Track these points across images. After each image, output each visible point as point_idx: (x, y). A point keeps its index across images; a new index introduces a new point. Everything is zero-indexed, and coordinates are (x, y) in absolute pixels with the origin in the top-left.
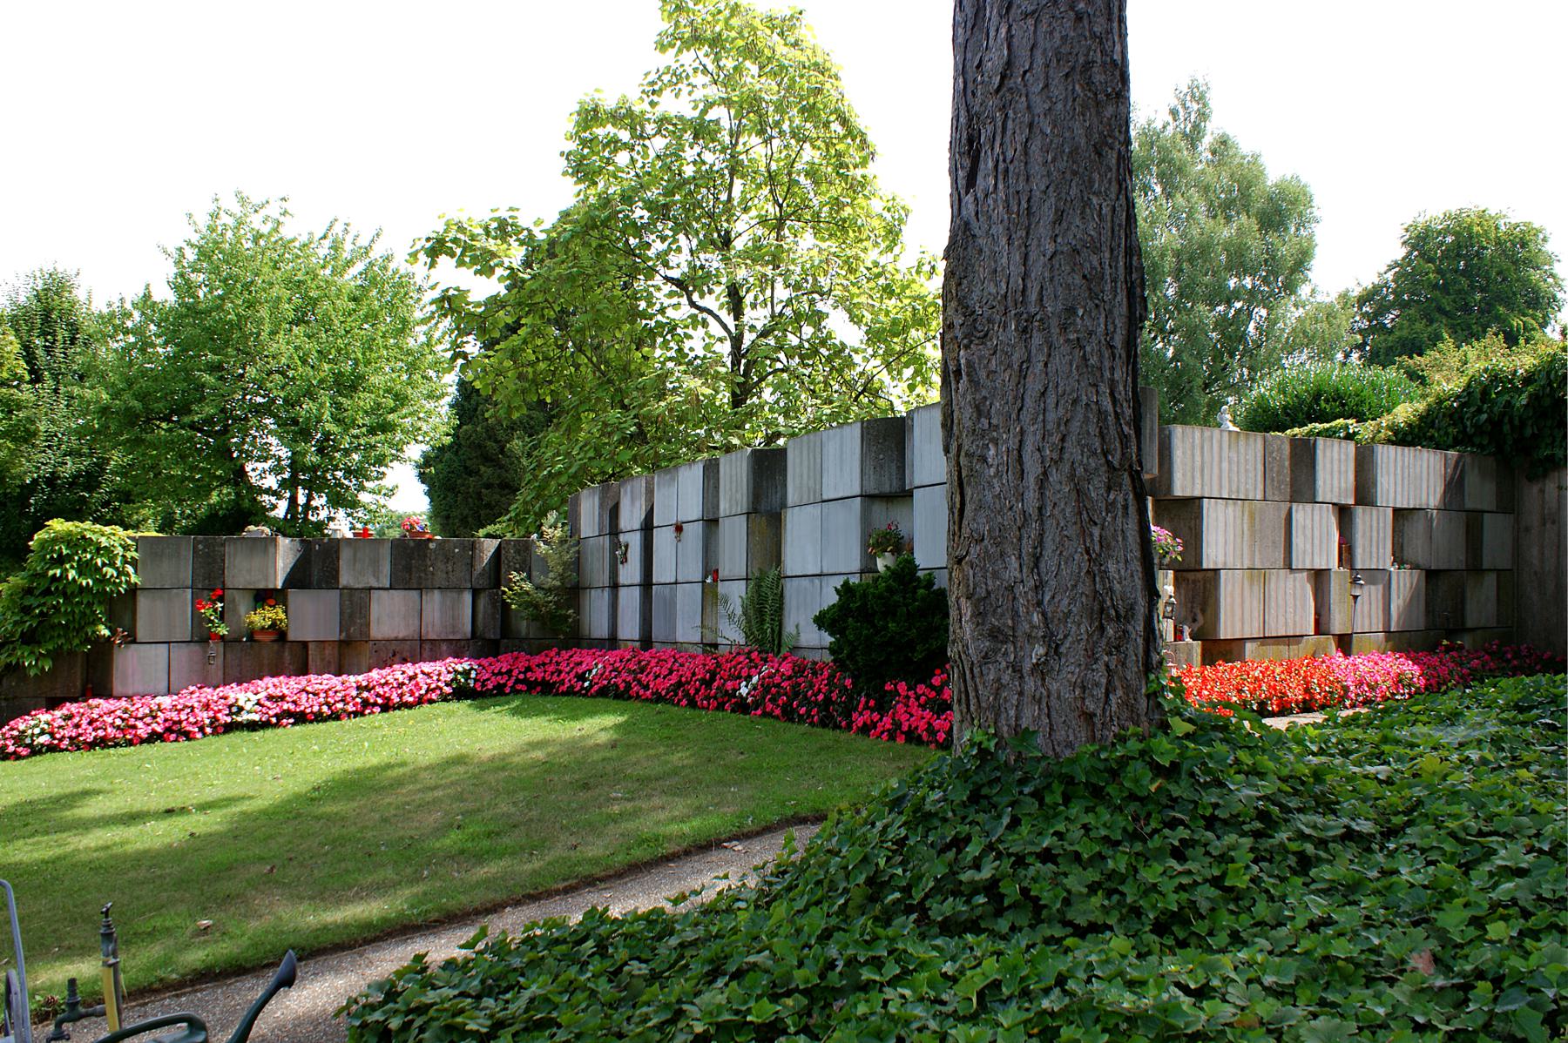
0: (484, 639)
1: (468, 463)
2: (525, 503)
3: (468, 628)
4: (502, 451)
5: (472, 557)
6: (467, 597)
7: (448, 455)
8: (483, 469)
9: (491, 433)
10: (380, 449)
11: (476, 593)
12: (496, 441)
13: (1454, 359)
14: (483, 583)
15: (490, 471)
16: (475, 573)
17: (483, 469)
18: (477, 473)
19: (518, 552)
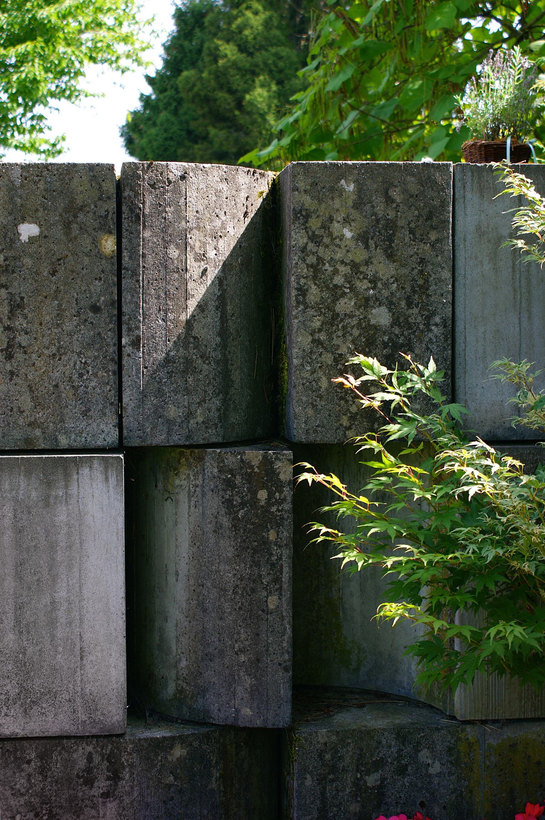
0: (200, 720)
1: (193, 125)
2: (318, 103)
3: (107, 667)
4: (239, 105)
5: (121, 269)
6: (98, 501)
7: (164, 115)
8: (212, 131)
9: (222, 79)
10: (34, 69)
11: (144, 475)
12: (231, 91)
13: (336, 225)
14: (189, 412)
15: (222, 134)
16: (142, 363)
17: (212, 131)
18: (205, 138)
19: (381, 235)
